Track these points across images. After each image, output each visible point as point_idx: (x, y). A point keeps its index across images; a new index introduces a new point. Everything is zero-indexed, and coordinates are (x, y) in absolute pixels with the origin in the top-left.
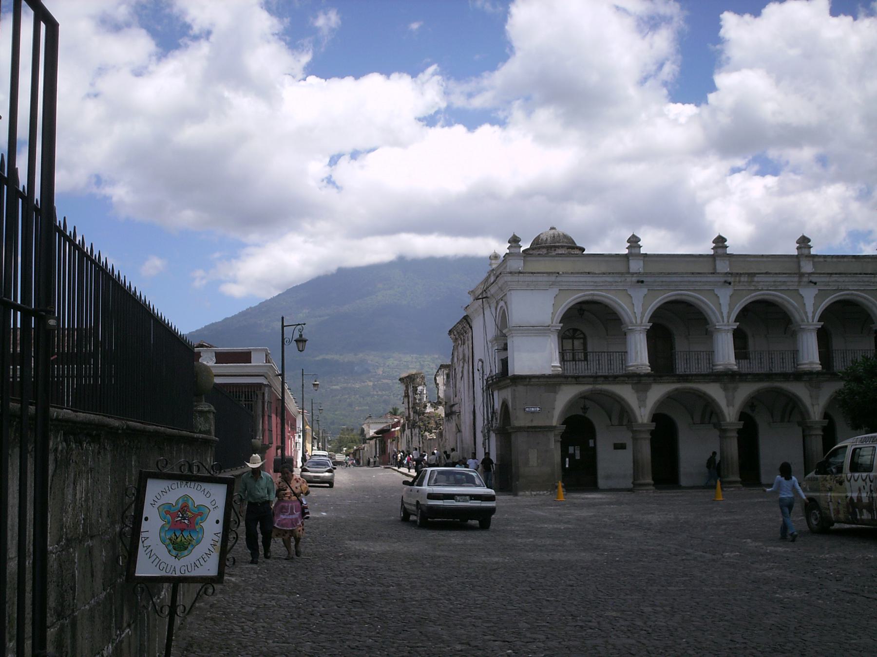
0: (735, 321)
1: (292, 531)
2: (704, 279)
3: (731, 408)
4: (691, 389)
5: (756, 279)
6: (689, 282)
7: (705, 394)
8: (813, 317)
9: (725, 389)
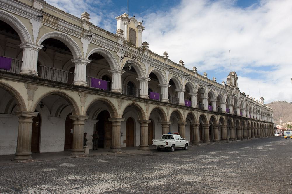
0: (42, 44)
1: (77, 163)
2: (23, 8)
3: (31, 102)
4: (62, 93)
5: (59, 22)
6: (12, 6)
7: (12, 89)
8: (86, 56)
9: (28, 88)
